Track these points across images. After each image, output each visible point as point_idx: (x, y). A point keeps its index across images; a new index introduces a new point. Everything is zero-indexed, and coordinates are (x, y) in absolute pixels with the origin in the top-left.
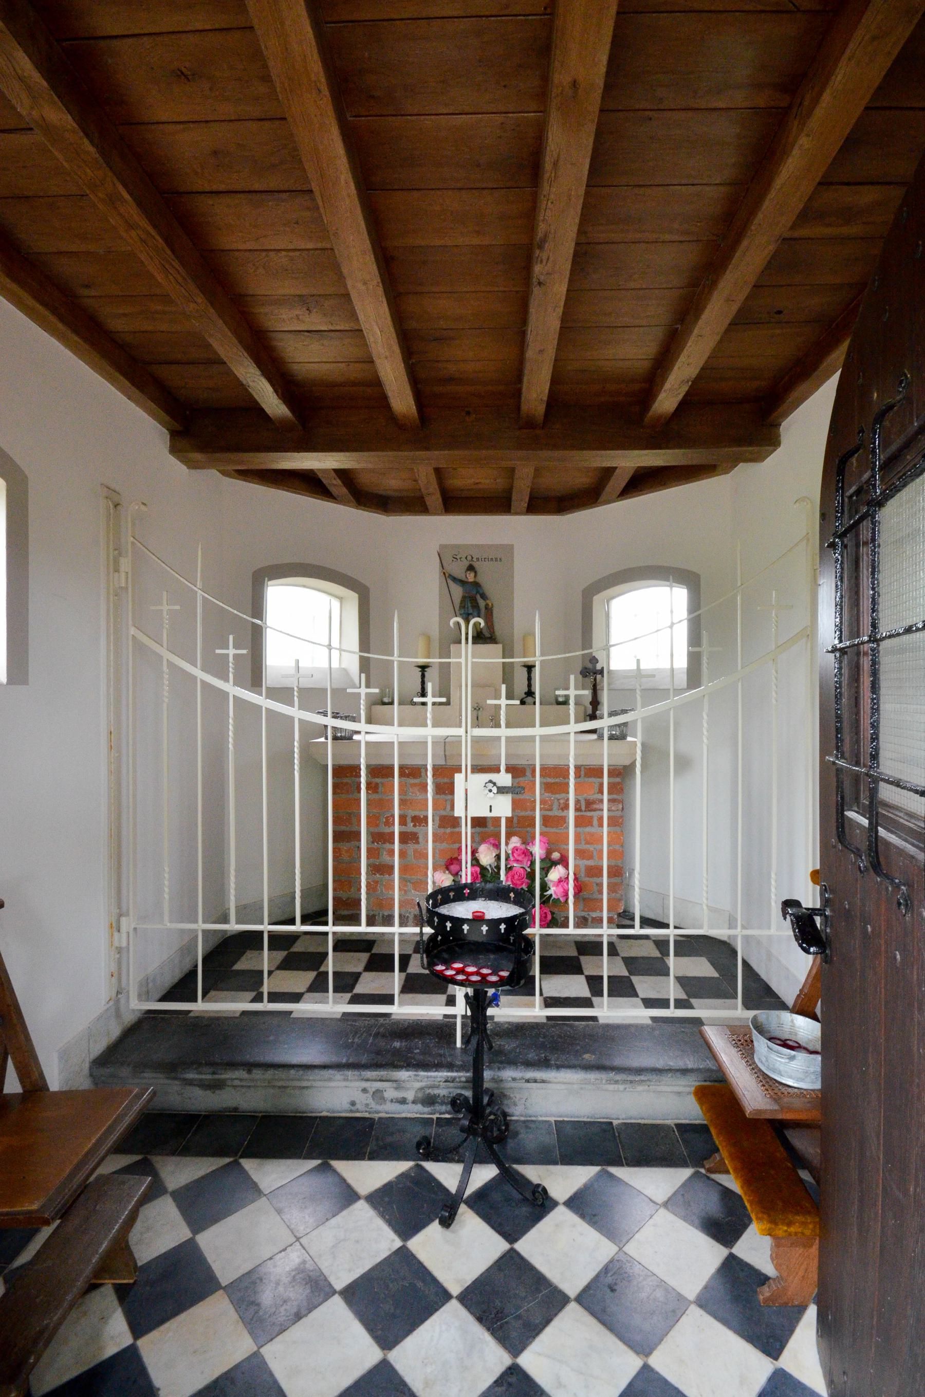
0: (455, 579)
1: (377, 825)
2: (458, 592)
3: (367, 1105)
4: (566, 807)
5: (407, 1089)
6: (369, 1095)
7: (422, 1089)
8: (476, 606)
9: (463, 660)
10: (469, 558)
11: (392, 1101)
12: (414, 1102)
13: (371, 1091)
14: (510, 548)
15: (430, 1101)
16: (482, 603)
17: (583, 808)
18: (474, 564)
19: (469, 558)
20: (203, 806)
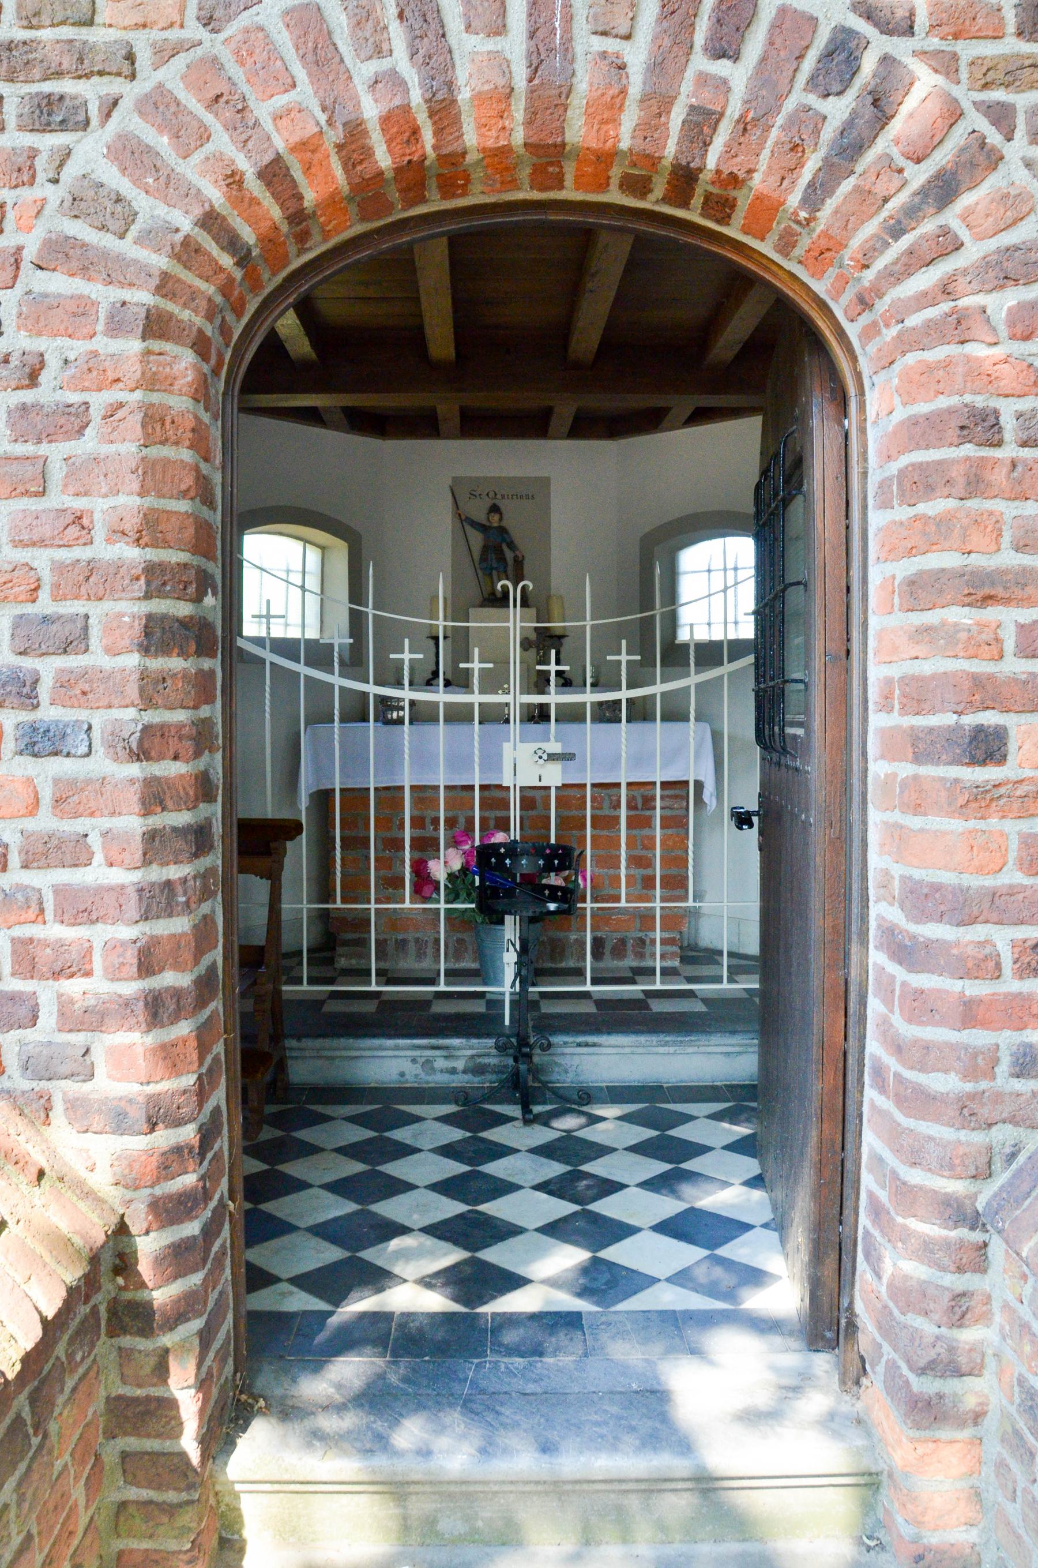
0: (474, 524)
1: (389, 829)
2: (477, 539)
3: (416, 1076)
4: (618, 805)
5: (457, 1057)
6: (419, 1066)
7: (472, 1057)
8: (502, 559)
9: (511, 625)
10: (492, 494)
11: (442, 1071)
12: (464, 1072)
13: (421, 1060)
14: (544, 483)
15: (479, 1070)
16: (509, 555)
17: (640, 806)
18: (497, 502)
19: (492, 494)
20: (592, 602)
